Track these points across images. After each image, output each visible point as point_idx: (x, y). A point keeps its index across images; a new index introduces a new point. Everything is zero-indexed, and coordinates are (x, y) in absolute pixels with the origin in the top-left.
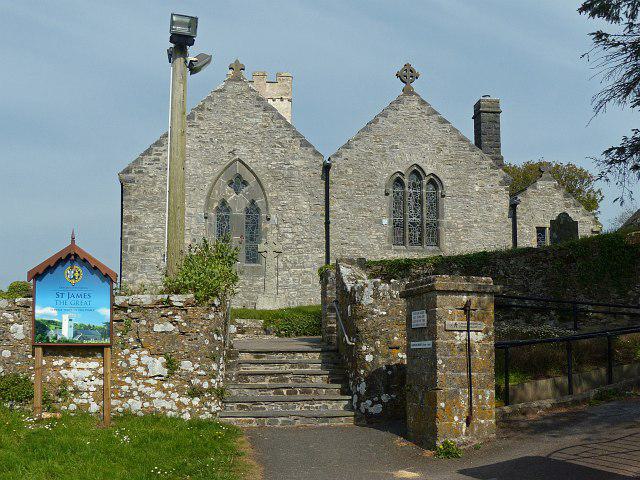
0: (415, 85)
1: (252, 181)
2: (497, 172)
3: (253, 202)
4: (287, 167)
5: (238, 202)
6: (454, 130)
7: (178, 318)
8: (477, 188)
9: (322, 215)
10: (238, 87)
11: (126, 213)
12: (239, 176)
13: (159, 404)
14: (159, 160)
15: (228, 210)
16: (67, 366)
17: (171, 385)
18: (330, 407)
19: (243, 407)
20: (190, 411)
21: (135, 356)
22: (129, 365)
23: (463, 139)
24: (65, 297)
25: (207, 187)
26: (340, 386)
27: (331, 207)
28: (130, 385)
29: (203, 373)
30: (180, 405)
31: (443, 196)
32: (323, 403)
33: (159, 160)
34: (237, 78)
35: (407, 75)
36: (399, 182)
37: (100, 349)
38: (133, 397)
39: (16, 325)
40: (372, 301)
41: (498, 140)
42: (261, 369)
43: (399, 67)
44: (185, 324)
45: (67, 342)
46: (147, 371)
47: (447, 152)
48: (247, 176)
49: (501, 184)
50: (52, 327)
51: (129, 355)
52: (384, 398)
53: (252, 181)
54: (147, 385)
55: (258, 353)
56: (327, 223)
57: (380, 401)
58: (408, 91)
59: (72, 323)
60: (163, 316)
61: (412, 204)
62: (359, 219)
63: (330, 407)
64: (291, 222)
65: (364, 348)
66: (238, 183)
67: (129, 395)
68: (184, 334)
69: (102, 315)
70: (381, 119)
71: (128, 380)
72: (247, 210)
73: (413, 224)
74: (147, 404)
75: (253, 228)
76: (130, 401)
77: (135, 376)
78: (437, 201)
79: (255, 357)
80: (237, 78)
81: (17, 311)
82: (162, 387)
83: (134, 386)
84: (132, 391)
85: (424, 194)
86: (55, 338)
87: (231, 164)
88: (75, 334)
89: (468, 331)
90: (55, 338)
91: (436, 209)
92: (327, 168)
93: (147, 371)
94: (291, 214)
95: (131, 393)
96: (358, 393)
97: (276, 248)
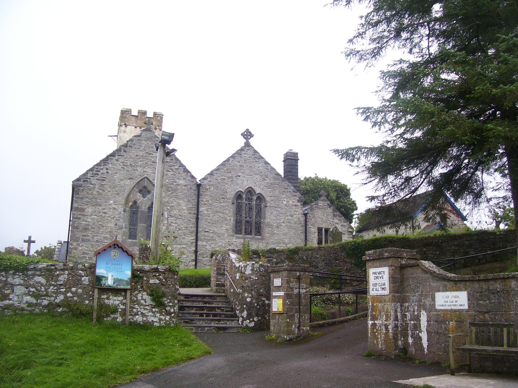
0: (252, 141)
2: (296, 194)
4: (175, 184)
7: (161, 277)
8: (285, 202)
9: (194, 214)
10: (149, 134)
11: (75, 205)
13: (151, 319)
14: (98, 175)
15: (138, 208)
16: (108, 298)
17: (157, 310)
21: (140, 295)
22: (137, 299)
23: (278, 174)
27: (201, 209)
28: (137, 309)
29: (171, 304)
30: (160, 319)
33: (98, 175)
34: (148, 130)
35: (247, 135)
36: (239, 196)
37: (125, 290)
38: (138, 315)
39: (85, 277)
42: (189, 304)
44: (164, 280)
45: (110, 286)
46: (145, 302)
47: (268, 181)
49: (298, 201)
51: (137, 294)
54: (145, 309)
56: (197, 219)
59: (113, 278)
62: (216, 218)
65: (246, 295)
67: (137, 314)
68: (163, 285)
71: (136, 306)
74: (145, 319)
76: (137, 317)
77: (139, 304)
79: (185, 298)
80: (148, 130)
81: (86, 270)
82: (152, 310)
83: (139, 310)
84: (138, 312)
87: (141, 180)
88: (114, 283)
89: (299, 288)
90: (105, 284)
91: (260, 212)
94: (175, 212)
95: (137, 313)
96: (242, 317)
97: (174, 235)
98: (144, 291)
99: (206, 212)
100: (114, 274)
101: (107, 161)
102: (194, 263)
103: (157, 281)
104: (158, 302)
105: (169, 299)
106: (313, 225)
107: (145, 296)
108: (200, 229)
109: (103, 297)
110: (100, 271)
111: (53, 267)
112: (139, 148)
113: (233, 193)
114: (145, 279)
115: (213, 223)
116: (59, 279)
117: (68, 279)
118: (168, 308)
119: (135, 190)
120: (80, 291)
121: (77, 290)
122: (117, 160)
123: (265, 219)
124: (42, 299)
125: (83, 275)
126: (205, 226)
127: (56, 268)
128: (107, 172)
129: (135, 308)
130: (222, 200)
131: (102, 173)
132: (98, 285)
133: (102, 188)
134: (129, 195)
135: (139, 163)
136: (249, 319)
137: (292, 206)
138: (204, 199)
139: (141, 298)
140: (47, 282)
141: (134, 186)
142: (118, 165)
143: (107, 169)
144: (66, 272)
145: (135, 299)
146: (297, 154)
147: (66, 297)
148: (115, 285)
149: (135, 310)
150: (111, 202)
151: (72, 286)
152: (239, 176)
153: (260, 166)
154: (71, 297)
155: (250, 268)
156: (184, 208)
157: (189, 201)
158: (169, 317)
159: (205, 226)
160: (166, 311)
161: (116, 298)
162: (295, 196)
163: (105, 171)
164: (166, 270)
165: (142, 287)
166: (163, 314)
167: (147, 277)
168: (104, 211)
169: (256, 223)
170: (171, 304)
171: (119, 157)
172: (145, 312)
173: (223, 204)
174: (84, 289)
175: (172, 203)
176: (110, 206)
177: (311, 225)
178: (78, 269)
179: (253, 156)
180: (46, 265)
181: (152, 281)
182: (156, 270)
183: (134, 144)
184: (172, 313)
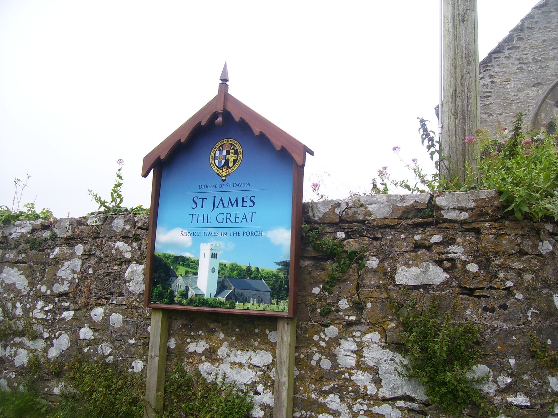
7: (457, 251)
16: (211, 355)
21: (348, 345)
22: (335, 365)
24: (208, 204)
44: (473, 268)
45: (205, 303)
46: (377, 382)
51: (335, 341)
59: (216, 263)
68: (470, 292)
81: (137, 238)
88: (221, 287)
90: (185, 295)
98: (374, 326)
101: (491, 62)
103: (437, 275)
105: (502, 369)
107: (376, 354)
109: (192, 348)
111: (47, 234)
112: (546, 27)
114: (373, 263)
116: (60, 273)
117: (83, 271)
119: (547, 103)
121: (107, 316)
122: (508, 58)
124: (15, 344)
125: (128, 256)
127: (54, 237)
128: (493, 82)
131: (484, 85)
132: (161, 296)
133: (486, 111)
134: (537, 115)
135: (551, 53)
139: (351, 361)
140: (32, 284)
141: (546, 97)
142: (510, 66)
143: (491, 76)
144: (80, 249)
145: (326, 364)
147: (75, 340)
151: (92, 300)
154: (89, 343)
161: (241, 357)
163: (488, 80)
164: (479, 213)
165: (358, 307)
167: (384, 255)
171: (510, 51)
174: (128, 310)
178: (113, 236)
180: (29, 228)
181: (406, 276)
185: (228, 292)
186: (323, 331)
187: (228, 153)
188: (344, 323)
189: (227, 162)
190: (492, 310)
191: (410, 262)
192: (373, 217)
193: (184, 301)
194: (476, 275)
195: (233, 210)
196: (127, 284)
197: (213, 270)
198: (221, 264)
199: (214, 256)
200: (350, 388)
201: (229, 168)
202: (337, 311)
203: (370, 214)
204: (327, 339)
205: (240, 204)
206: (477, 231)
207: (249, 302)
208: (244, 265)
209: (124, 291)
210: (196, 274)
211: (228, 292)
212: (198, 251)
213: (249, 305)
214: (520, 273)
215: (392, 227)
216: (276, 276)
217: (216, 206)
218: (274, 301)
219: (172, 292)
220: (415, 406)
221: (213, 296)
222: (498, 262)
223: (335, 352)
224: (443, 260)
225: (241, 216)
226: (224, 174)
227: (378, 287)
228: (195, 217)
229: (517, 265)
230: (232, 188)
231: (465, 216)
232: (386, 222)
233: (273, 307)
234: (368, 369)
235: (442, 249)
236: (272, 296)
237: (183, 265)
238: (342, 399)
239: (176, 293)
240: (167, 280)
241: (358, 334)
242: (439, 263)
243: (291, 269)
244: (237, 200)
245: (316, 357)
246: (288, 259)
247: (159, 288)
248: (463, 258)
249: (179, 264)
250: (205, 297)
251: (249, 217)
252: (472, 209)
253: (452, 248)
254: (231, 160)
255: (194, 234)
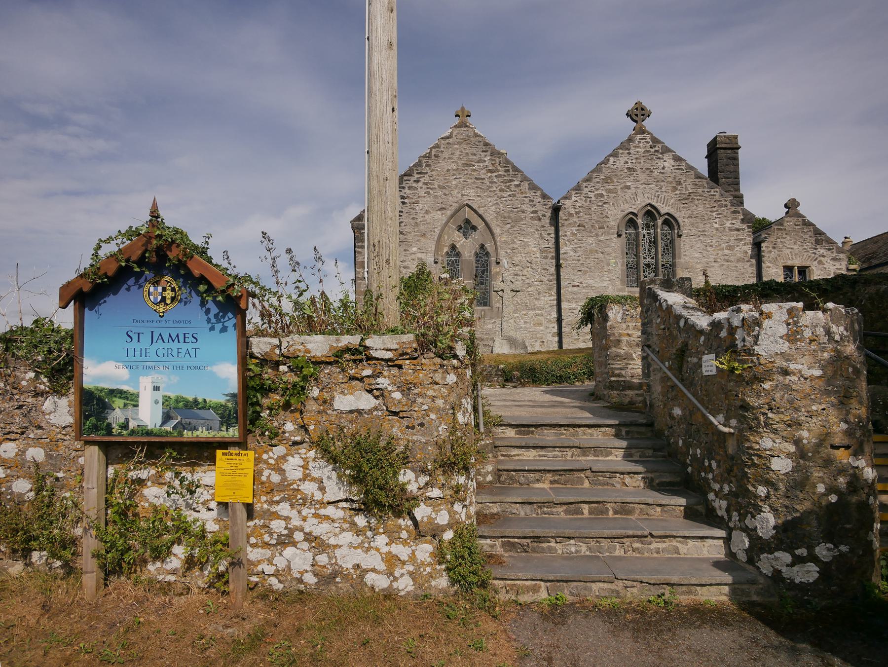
0: (648, 124)
1: (481, 225)
3: (482, 246)
5: (468, 247)
6: (690, 168)
7: (383, 382)
12: (467, 221)
13: (348, 559)
15: (458, 254)
18: (683, 549)
19: (513, 545)
20: (411, 574)
22: (284, 479)
23: (699, 176)
24: (146, 339)
25: (437, 231)
26: (682, 501)
27: (563, 250)
28: (287, 519)
29: (435, 493)
30: (392, 561)
31: (680, 236)
32: (668, 543)
34: (463, 125)
36: (631, 222)
38: (294, 544)
40: (785, 347)
41: (737, 178)
43: (630, 105)
44: (397, 395)
45: (149, 433)
46: (322, 489)
48: (475, 221)
50: (118, 403)
51: (284, 458)
52: (823, 551)
53: (481, 225)
55: (522, 427)
56: (558, 267)
57: (813, 558)
58: (641, 131)
59: (159, 395)
60: (352, 378)
61: (646, 245)
63: (683, 549)
64: (521, 256)
66: (467, 227)
67: (285, 541)
68: (395, 414)
69: (221, 378)
70: (612, 160)
71: (284, 509)
72: (476, 254)
73: (648, 265)
75: (483, 272)
76: (289, 551)
77: (296, 498)
78: (672, 242)
82: (353, 524)
83: (296, 522)
84: (291, 531)
85: (659, 235)
86: (125, 426)
88: (167, 418)
90: (125, 426)
92: (556, 210)
93: (322, 489)
95: (290, 535)
97: (513, 287)
99: (572, 254)
100: (161, 378)
102: (556, 339)
104: (377, 498)
106: (775, 261)
108: (563, 284)
110: (98, 371)
113: (620, 215)
114: (315, 392)
115: (586, 272)
118: (421, 512)
119: (450, 227)
120: (36, 454)
123: (680, 258)
126: (574, 277)
129: (276, 516)
130: (600, 232)
132: (95, 428)
134: (440, 236)
135: (454, 182)
136: (790, 549)
137: (731, 230)
138: (567, 231)
145: (276, 478)
146: (736, 137)
148: (169, 428)
149: (278, 526)
150: (415, 249)
152: (629, 188)
153: (668, 163)
155: (783, 330)
156: (535, 249)
157: (541, 237)
158: (429, 548)
159: (574, 277)
160: (416, 523)
162: (734, 212)
166: (404, 535)
168: (404, 264)
169: (663, 265)
170: (435, 493)
172: (321, 530)
173: (602, 238)
174: (51, 445)
175: (514, 242)
176: (413, 256)
177: (771, 262)
179: (652, 150)
182: (360, 354)
183: (442, 152)
184: (443, 529)
185: (174, 422)
186: (271, 450)
187: (164, 289)
188: (291, 443)
189: (164, 299)
190: (413, 428)
191: (346, 392)
192: (312, 354)
193: (125, 432)
194: (399, 402)
195: (175, 346)
196: (47, 417)
197: (156, 402)
198: (164, 397)
199: (156, 388)
200: (299, 497)
201: (166, 304)
202: (284, 433)
203: (309, 352)
204: (275, 457)
205: (182, 340)
206: (400, 367)
207: (198, 430)
208: (190, 398)
209: (43, 424)
210: (137, 406)
211: (174, 422)
212: (137, 383)
213: (196, 433)
214: (433, 398)
215: (330, 363)
216: (225, 406)
217: (155, 340)
218: (224, 428)
219: (109, 425)
220: (355, 506)
221: (158, 427)
222: (416, 391)
223: (283, 467)
224: (372, 390)
225: (183, 351)
226: (162, 310)
227: (319, 412)
228: (131, 352)
229: (430, 393)
230: (171, 324)
231: (389, 355)
232: (323, 359)
233: (224, 433)
234: (313, 479)
235: (372, 381)
236: (222, 424)
237: (120, 398)
238: (292, 506)
239: (114, 426)
240: (102, 412)
241: (303, 451)
242: (370, 391)
243: (240, 400)
244: (178, 335)
245: (266, 473)
246: (236, 391)
247: (92, 420)
248: (389, 388)
249: (115, 396)
250: (149, 428)
251: (192, 353)
252: (395, 350)
253: (379, 380)
254: (168, 297)
255: (131, 367)
